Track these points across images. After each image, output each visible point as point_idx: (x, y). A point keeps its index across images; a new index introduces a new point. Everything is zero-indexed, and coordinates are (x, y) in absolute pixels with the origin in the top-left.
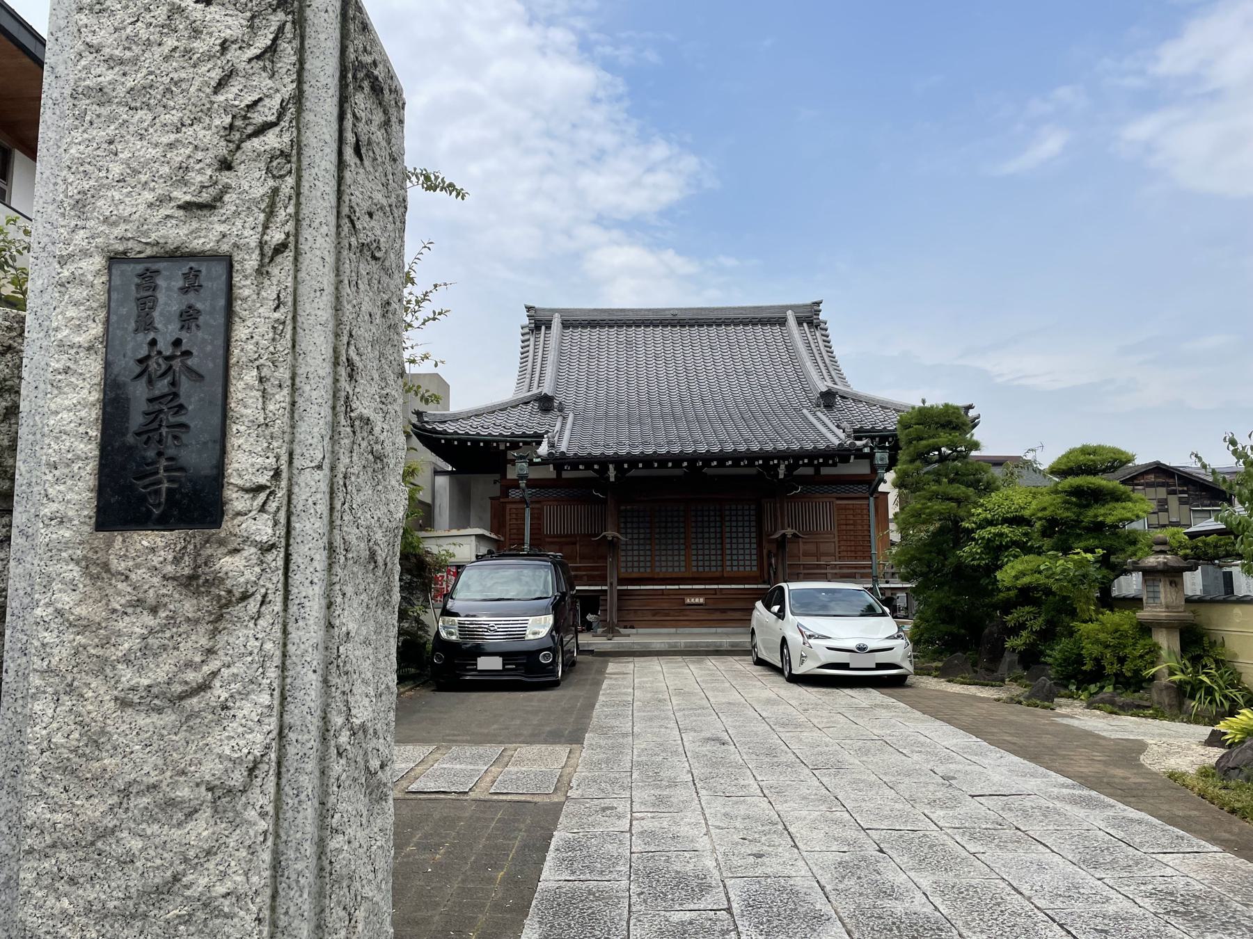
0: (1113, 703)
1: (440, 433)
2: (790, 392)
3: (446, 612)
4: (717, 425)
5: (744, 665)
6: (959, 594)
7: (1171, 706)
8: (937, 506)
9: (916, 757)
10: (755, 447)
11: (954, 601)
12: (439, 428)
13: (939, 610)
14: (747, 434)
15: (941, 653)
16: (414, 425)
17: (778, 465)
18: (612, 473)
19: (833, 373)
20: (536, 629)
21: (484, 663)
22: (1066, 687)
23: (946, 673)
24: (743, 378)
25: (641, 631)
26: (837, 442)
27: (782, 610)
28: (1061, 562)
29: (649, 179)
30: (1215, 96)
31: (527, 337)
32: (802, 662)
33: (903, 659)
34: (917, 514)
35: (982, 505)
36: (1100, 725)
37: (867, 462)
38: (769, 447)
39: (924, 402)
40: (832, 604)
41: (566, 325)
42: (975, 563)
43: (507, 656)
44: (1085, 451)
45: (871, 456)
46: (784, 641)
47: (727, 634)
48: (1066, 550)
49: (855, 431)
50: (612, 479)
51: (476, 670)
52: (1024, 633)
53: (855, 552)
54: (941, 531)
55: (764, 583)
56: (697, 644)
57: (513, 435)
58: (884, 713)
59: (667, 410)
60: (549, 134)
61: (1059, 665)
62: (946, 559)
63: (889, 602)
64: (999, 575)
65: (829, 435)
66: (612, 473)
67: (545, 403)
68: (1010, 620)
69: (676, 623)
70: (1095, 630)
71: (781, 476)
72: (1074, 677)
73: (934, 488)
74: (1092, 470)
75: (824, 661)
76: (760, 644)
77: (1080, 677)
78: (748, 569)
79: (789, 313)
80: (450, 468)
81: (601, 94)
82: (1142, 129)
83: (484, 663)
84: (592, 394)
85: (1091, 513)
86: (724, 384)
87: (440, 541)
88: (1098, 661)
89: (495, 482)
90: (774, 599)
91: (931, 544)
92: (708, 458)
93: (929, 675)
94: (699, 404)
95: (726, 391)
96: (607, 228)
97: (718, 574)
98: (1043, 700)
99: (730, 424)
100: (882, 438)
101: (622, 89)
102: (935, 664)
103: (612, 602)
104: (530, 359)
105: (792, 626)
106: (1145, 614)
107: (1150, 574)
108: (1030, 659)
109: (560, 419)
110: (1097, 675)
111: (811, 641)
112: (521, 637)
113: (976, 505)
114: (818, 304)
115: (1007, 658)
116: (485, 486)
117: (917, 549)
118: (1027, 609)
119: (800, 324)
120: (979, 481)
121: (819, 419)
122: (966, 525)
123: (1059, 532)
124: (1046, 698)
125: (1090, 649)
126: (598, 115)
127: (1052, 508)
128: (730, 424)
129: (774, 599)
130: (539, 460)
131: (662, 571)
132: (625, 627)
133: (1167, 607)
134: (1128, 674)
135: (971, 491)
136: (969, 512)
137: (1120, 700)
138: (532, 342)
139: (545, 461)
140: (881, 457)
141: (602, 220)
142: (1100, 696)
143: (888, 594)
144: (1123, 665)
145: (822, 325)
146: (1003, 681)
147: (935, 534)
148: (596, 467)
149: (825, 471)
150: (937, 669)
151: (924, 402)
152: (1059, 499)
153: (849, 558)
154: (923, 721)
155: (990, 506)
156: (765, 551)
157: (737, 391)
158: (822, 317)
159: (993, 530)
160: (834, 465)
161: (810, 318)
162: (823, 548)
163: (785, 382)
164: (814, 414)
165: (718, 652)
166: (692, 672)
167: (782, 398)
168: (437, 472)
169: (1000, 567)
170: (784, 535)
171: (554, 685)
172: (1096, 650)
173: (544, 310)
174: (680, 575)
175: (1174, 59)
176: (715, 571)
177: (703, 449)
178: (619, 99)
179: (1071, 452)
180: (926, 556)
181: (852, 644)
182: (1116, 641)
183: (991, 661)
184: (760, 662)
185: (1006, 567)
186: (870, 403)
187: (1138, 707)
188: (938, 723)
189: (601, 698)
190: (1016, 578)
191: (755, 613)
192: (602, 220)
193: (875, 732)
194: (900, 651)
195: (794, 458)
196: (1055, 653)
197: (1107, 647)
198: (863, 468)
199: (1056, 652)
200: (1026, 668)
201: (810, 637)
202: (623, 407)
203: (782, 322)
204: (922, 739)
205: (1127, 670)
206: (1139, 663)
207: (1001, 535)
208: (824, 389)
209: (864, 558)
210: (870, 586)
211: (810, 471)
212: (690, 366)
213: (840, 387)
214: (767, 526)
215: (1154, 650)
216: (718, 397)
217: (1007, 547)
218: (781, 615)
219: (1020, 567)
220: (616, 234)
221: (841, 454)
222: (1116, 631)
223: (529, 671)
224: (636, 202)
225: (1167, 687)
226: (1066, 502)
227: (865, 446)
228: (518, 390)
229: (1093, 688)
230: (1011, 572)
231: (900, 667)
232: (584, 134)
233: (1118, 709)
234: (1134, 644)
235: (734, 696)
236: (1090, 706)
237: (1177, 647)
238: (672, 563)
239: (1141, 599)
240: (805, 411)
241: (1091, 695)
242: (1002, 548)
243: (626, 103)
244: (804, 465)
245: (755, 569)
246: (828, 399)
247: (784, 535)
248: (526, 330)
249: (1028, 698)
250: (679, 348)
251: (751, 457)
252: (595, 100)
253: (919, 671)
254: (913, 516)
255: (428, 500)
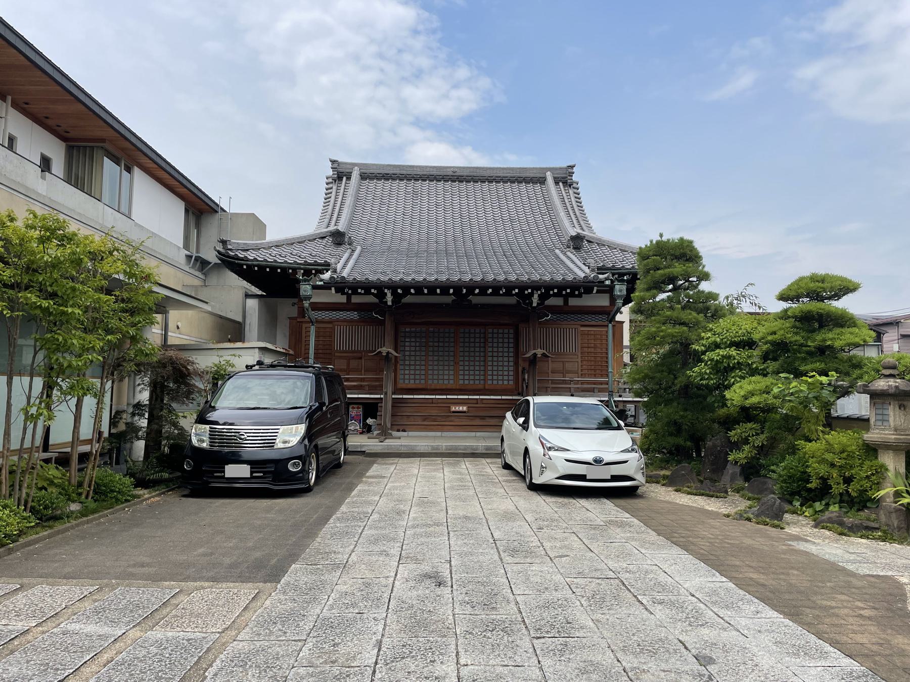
0: (841, 524)
1: (242, 259)
2: (546, 236)
3: (202, 419)
4: (483, 259)
5: (492, 468)
6: (686, 410)
7: (899, 529)
8: (670, 330)
9: (660, 612)
10: (513, 278)
11: (682, 417)
12: (241, 255)
13: (668, 424)
14: (507, 268)
15: (667, 462)
16: (219, 252)
17: (532, 294)
18: (389, 298)
19: (582, 223)
20: (287, 438)
21: (233, 471)
22: (791, 503)
23: (671, 482)
24: (508, 224)
25: (411, 433)
26: (582, 275)
27: (526, 422)
28: (794, 384)
29: (455, 93)
30: (863, 49)
31: (330, 186)
32: (542, 473)
33: (636, 472)
34: (651, 337)
35: (711, 330)
36: (839, 552)
37: (607, 295)
38: (525, 278)
39: (661, 235)
40: (573, 418)
41: (364, 177)
42: (704, 382)
43: (255, 464)
44: (814, 278)
45: (610, 290)
46: (526, 451)
47: (484, 438)
48: (798, 374)
49: (599, 269)
50: (390, 303)
51: (223, 477)
52: (746, 448)
53: (595, 370)
54: (672, 353)
55: (519, 394)
56: (456, 448)
57: (306, 263)
58: (618, 534)
59: (442, 247)
60: (381, 56)
61: (784, 481)
62: (676, 378)
63: (621, 414)
64: (728, 394)
65: (576, 270)
66: (389, 298)
67: (338, 238)
68: (734, 434)
69: (441, 428)
70: (819, 450)
71: (535, 305)
72: (798, 493)
73: (668, 313)
74: (816, 296)
75: (563, 472)
76: (507, 451)
77: (804, 494)
78: (506, 383)
79: (548, 174)
80: (260, 293)
81: (421, 27)
82: (810, 71)
83: (233, 471)
84: (380, 233)
85: (819, 337)
86: (492, 228)
87: (221, 353)
88: (824, 480)
89: (294, 304)
90: (522, 410)
91: (662, 365)
92: (471, 287)
93: (658, 482)
94: (469, 243)
95: (493, 233)
96: (423, 129)
97: (481, 387)
98: (772, 518)
99: (493, 260)
100: (619, 274)
101: (436, 24)
102: (663, 472)
103: (386, 410)
104: (331, 204)
105: (535, 437)
106: (873, 436)
107: (877, 397)
108: (751, 471)
109: (349, 251)
110: (823, 492)
111: (551, 453)
112: (270, 444)
113: (706, 330)
114: (572, 167)
115: (730, 469)
116: (286, 309)
117: (650, 368)
118: (749, 425)
119: (557, 183)
120: (708, 308)
121: (568, 257)
122: (695, 347)
123: (782, 355)
124: (773, 516)
125: (816, 469)
126: (418, 43)
127: (782, 332)
128: (493, 260)
129: (522, 410)
130: (322, 283)
131: (433, 384)
132: (398, 431)
133: (896, 430)
134: (854, 494)
135: (701, 317)
136: (699, 335)
137: (849, 520)
138: (334, 190)
139: (327, 286)
140: (620, 289)
141: (420, 123)
142: (827, 514)
143: (621, 407)
144: (849, 485)
145: (575, 185)
146: (726, 492)
147: (665, 357)
148: (373, 291)
149: (573, 302)
150: (665, 477)
151: (661, 235)
152: (788, 324)
153: (590, 375)
154: (660, 547)
155: (719, 330)
156: (520, 369)
157: (502, 234)
158: (574, 178)
159: (722, 352)
160: (580, 296)
161: (565, 179)
162: (569, 366)
163: (543, 229)
164: (565, 254)
165: (474, 455)
166: (445, 474)
167: (539, 241)
168: (247, 296)
169: (728, 387)
170: (535, 355)
171: (308, 490)
172: (823, 470)
173: (346, 163)
174: (449, 387)
175: (835, 21)
176: (479, 384)
177: (467, 278)
178: (434, 31)
179: (801, 279)
180: (658, 375)
181: (589, 457)
182: (843, 462)
183: (713, 471)
184: (507, 466)
185: (734, 387)
186: (612, 246)
187: (867, 528)
188: (676, 551)
189: (344, 508)
190: (746, 398)
191: (506, 423)
192: (420, 123)
193: (611, 564)
194: (634, 465)
195: (547, 289)
196: (779, 470)
197: (833, 465)
198: (603, 301)
199: (781, 468)
200: (747, 479)
201: (550, 449)
202: (405, 244)
203: (542, 181)
204: (662, 578)
205: (853, 489)
206: (867, 484)
207: (729, 357)
208: (574, 234)
209: (602, 376)
210: (606, 399)
211: (559, 302)
212: (465, 214)
213: (586, 233)
214: (522, 348)
215: (881, 471)
216: (486, 238)
217: (733, 369)
218: (525, 426)
219: (750, 388)
220: (429, 133)
221: (585, 287)
222: (843, 452)
223: (277, 479)
224: (445, 109)
225: (897, 510)
226: (794, 327)
227: (607, 279)
228: (318, 227)
229: (818, 506)
230: (738, 392)
231: (634, 480)
232: (407, 57)
233: (845, 530)
234: (861, 465)
235: (474, 509)
236: (818, 525)
237: (902, 470)
238: (447, 379)
239: (868, 420)
240: (557, 251)
241: (816, 512)
242: (729, 369)
243: (439, 35)
244: (555, 295)
245: (511, 383)
246: (577, 242)
247: (535, 355)
248: (330, 180)
249: (757, 516)
250: (456, 198)
251: (509, 287)
252: (415, 32)
253: (650, 479)
254: (648, 339)
255: (240, 319)
